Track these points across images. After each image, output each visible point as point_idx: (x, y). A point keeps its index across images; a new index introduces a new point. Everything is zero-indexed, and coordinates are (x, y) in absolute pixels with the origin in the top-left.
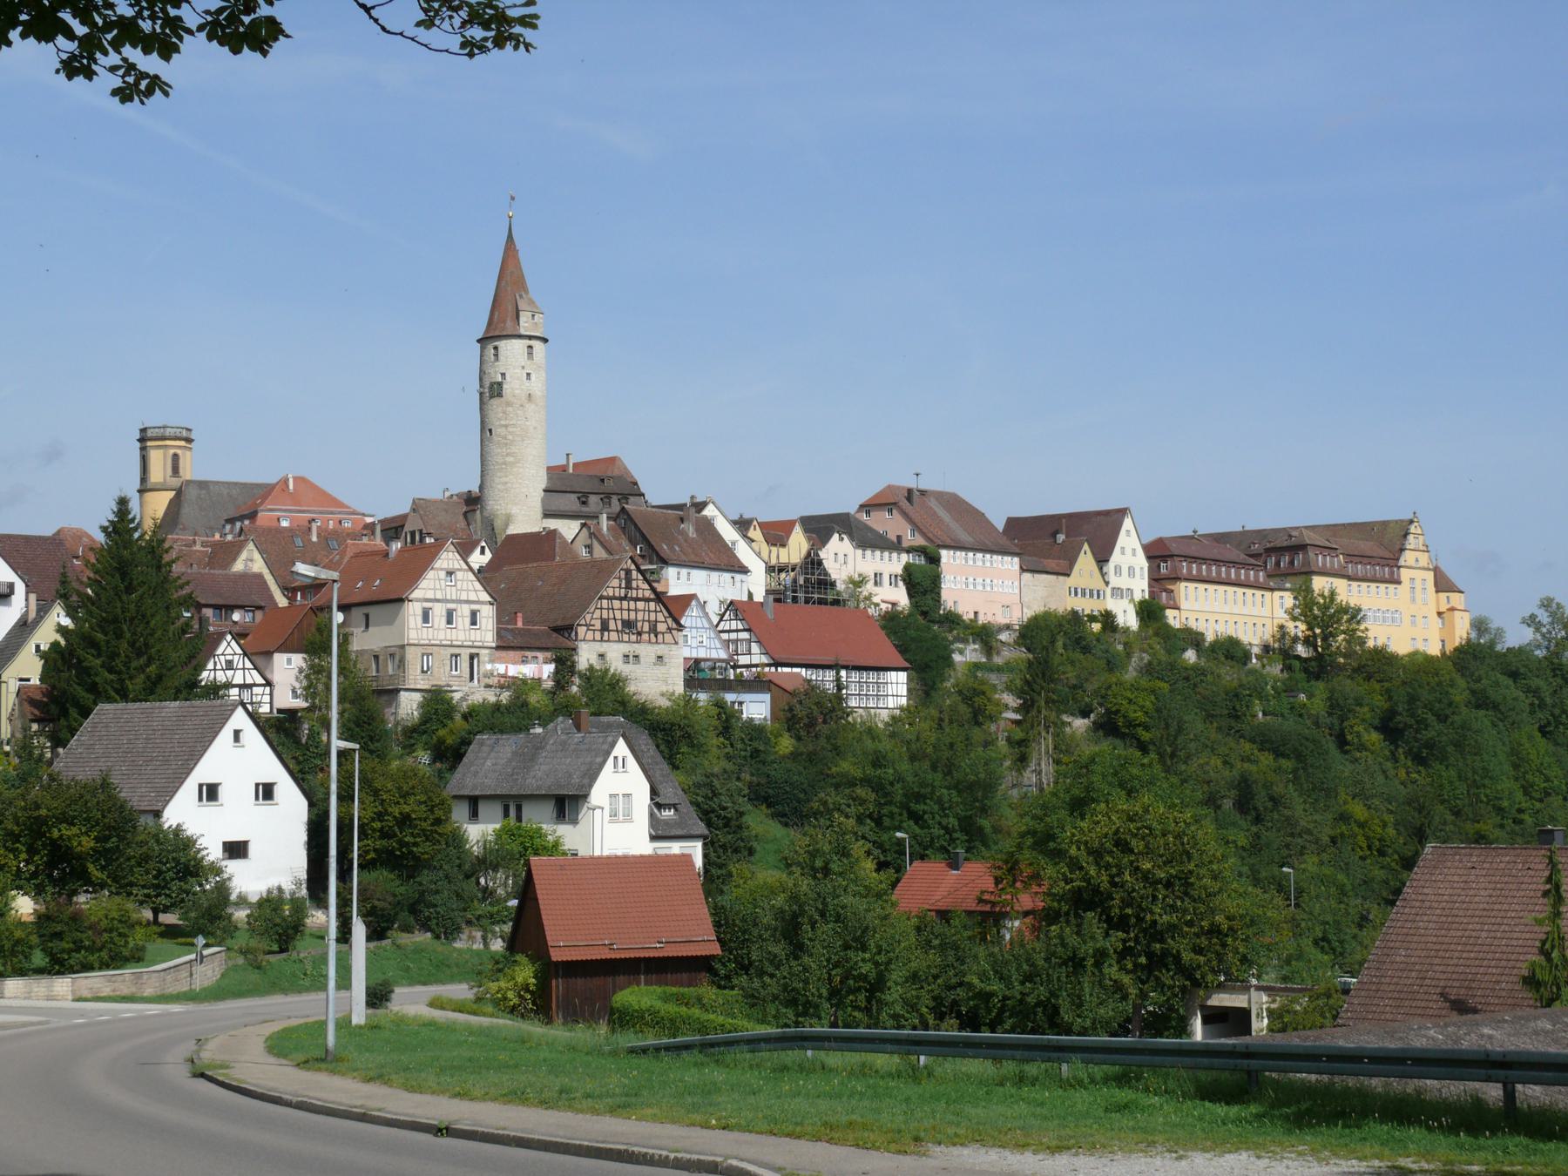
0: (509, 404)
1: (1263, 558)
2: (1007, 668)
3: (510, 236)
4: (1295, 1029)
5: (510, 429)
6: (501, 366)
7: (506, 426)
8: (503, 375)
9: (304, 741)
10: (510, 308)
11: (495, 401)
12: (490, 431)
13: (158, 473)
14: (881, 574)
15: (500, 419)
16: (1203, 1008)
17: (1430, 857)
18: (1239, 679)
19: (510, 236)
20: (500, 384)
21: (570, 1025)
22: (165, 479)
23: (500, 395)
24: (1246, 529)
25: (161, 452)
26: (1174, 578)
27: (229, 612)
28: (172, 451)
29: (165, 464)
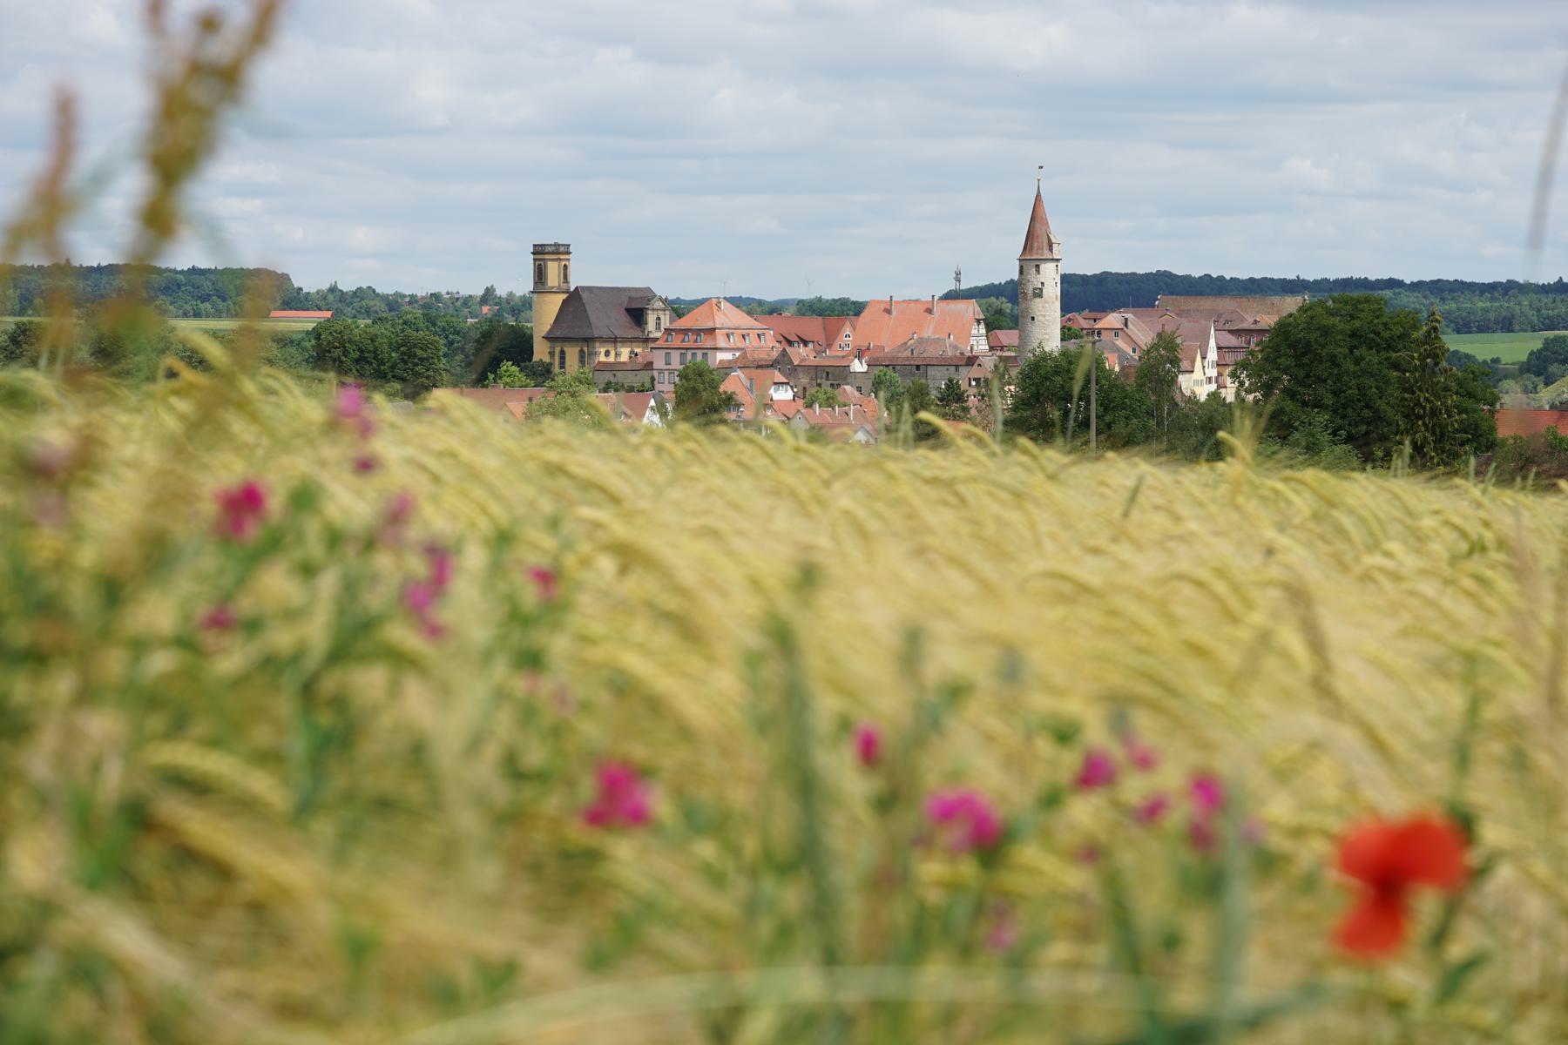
0: (1046, 302)
1: (656, 374)
2: (671, 372)
3: (1038, 197)
4: (616, 390)
7: (1045, 316)
8: (1043, 284)
9: (328, 314)
11: (1038, 300)
12: (1033, 318)
13: (553, 278)
14: (535, 246)
15: (1040, 311)
18: (1329, 434)
19: (1038, 197)
20: (1041, 290)
21: (418, 398)
22: (559, 284)
23: (1040, 296)
25: (556, 263)
26: (1223, 365)
28: (563, 263)
29: (559, 276)
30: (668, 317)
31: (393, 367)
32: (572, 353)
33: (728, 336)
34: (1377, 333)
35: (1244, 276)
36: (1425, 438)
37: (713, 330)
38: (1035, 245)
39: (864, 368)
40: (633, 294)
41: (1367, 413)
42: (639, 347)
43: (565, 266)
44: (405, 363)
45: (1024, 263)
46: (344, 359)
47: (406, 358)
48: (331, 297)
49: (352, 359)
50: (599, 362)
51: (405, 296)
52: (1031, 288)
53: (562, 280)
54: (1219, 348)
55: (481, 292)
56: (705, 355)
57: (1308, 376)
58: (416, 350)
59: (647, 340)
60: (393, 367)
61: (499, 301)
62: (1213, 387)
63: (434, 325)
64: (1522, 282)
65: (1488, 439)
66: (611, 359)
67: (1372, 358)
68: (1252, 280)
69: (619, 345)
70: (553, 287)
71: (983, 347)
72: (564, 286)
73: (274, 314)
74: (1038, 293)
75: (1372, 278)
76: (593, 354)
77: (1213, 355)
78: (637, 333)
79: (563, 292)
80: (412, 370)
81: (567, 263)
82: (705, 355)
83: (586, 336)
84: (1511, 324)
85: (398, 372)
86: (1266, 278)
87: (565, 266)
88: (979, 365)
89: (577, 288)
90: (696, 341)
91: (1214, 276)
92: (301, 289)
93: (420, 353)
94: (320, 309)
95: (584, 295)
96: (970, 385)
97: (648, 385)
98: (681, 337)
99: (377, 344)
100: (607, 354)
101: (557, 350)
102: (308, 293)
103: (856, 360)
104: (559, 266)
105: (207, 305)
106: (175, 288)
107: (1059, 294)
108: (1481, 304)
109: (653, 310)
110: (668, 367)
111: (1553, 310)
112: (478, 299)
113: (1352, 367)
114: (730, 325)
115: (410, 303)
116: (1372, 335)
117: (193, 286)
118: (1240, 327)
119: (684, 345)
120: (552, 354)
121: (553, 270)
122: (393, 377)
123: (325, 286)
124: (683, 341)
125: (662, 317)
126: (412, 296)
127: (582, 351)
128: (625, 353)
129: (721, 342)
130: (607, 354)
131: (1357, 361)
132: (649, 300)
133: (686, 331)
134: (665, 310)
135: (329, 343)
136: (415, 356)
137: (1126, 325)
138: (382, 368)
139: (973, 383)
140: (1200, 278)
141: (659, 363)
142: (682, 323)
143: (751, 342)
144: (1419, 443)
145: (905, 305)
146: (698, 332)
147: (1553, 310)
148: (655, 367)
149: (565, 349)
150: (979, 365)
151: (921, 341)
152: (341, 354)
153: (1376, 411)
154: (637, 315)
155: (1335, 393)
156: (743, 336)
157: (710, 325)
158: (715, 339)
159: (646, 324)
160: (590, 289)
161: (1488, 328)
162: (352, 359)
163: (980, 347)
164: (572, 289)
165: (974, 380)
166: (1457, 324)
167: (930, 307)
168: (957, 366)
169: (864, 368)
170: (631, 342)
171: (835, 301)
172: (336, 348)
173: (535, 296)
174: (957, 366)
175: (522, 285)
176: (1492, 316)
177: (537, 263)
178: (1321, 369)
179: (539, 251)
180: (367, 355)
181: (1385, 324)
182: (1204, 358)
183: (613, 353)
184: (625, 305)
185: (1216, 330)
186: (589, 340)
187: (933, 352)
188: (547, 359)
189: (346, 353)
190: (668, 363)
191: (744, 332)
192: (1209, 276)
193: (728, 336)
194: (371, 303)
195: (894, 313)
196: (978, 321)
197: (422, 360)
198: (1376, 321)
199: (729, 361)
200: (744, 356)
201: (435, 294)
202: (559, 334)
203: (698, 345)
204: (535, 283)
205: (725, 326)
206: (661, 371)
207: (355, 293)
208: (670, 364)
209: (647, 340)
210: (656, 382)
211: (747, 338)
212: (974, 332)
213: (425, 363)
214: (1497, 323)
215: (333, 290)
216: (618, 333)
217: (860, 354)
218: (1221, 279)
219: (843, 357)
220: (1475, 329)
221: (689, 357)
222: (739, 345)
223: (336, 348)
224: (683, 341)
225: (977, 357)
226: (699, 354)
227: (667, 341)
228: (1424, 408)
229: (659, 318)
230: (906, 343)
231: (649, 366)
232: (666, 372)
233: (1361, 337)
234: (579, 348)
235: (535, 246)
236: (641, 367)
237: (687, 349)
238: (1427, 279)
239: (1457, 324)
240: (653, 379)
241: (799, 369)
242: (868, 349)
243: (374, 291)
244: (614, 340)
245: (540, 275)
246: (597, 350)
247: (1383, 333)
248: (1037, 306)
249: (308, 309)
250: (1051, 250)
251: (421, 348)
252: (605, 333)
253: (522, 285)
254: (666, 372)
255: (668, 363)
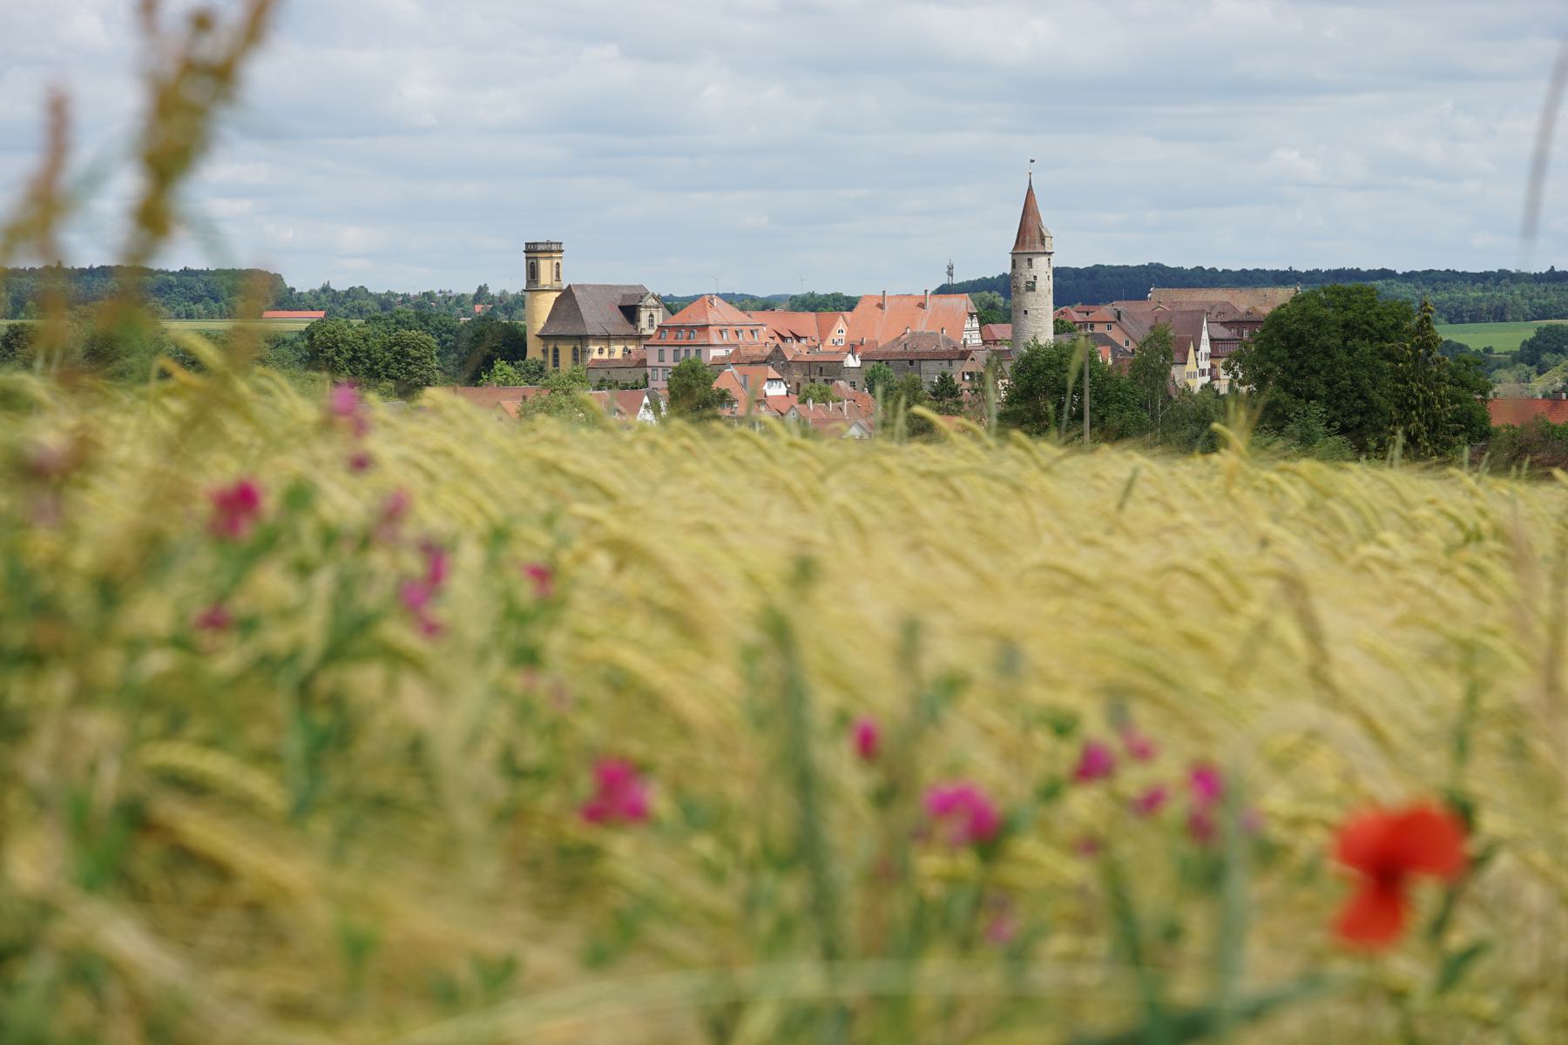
1: (649, 371)
2: (665, 368)
3: (1030, 189)
5: (1040, 311)
6: (1034, 272)
8: (1035, 277)
10: (1037, 234)
11: (1030, 293)
12: (1026, 312)
14: (527, 244)
16: (555, 346)
17: (1443, 392)
19: (1030, 189)
20: (1034, 283)
23: (1033, 289)
24: (1557, 270)
25: (548, 262)
27: (709, 372)
28: (556, 261)
30: (661, 314)
31: (386, 367)
32: (566, 351)
33: (721, 332)
34: (1369, 324)
35: (1236, 268)
36: (1419, 428)
37: (707, 326)
38: (1028, 238)
39: (858, 363)
40: (625, 291)
41: (1360, 404)
42: (630, 345)
43: (558, 264)
44: (399, 362)
45: (1017, 257)
46: (336, 358)
47: (399, 357)
48: (323, 297)
49: (345, 359)
50: (593, 360)
51: (397, 295)
52: (1024, 282)
53: (555, 278)
54: (1212, 340)
55: (474, 291)
56: (698, 352)
57: (1301, 367)
58: (409, 350)
59: (639, 338)
60: (386, 367)
61: (492, 299)
62: (1207, 379)
63: (427, 324)
64: (1513, 271)
65: (1481, 428)
66: (605, 356)
67: (1365, 348)
68: (1244, 271)
69: (612, 342)
70: (545, 286)
71: (977, 341)
72: (557, 285)
73: (267, 314)
74: (1031, 287)
75: (1364, 269)
76: (585, 352)
77: (1205, 347)
78: (630, 330)
79: (556, 291)
80: (405, 369)
81: (559, 261)
82: (698, 352)
83: (579, 333)
84: (1503, 314)
85: (393, 372)
86: (1257, 270)
87: (558, 264)
88: (972, 359)
89: (569, 286)
90: (689, 338)
91: (1206, 268)
92: (293, 289)
93: (413, 352)
94: (313, 310)
95: (577, 293)
96: (963, 379)
97: (641, 382)
98: (674, 334)
99: (370, 343)
100: (601, 351)
101: (551, 348)
102: (301, 294)
103: (850, 356)
104: (552, 264)
105: (200, 306)
106: (167, 289)
107: (1052, 288)
108: (1473, 294)
109: (646, 307)
110: (662, 364)
111: (1545, 298)
112: (471, 298)
113: (1345, 358)
114: (723, 321)
115: (403, 302)
116: (1365, 327)
117: (185, 287)
118: (1233, 318)
119: (679, 342)
120: (545, 352)
121: (545, 268)
122: (387, 376)
123: (318, 286)
124: (676, 338)
125: (655, 314)
126: (404, 295)
127: (575, 349)
128: (618, 351)
129: (715, 339)
130: (601, 351)
131: (1350, 352)
132: (642, 298)
133: (678, 328)
134: (658, 308)
135: (322, 343)
136: (408, 355)
137: (1119, 318)
138: (376, 367)
139: (967, 377)
140: (1192, 270)
141: (652, 360)
142: (675, 320)
143: (745, 338)
144: (1412, 433)
145: (898, 300)
146: (691, 329)
147: (1545, 298)
148: (648, 365)
149: (558, 346)
150: (972, 359)
151: (914, 336)
152: (334, 354)
153: (1369, 401)
154: (630, 312)
155: (1329, 384)
156: (737, 333)
157: (703, 321)
158: (708, 336)
159: (639, 321)
160: (582, 287)
161: (1481, 318)
162: (345, 359)
163: (974, 341)
164: (565, 287)
165: (968, 374)
166: (1449, 313)
167: (922, 301)
168: (950, 360)
169: (858, 363)
170: (624, 339)
171: (828, 296)
172: (329, 348)
173: (528, 294)
174: (950, 360)
175: (515, 283)
176: (1484, 305)
177: (530, 261)
178: (1314, 361)
179: (532, 250)
180: (360, 354)
181: (1378, 315)
182: (1197, 350)
183: (606, 351)
184: (619, 303)
185: (1208, 322)
186: (583, 339)
187: (926, 346)
188: (540, 357)
189: (339, 353)
190: (661, 360)
191: (738, 328)
192: (1201, 268)
193: (721, 332)
194: (363, 303)
195: (887, 308)
196: (971, 315)
197: (416, 359)
198: (1368, 312)
199: (722, 358)
200: (737, 352)
201: (428, 293)
202: (552, 332)
203: (692, 341)
204: (528, 282)
205: (718, 322)
206: (654, 368)
207: (348, 293)
208: (663, 361)
209: (639, 338)
210: (649, 379)
211: (725, 334)
212: (967, 326)
213: (418, 362)
214: (1489, 312)
215: (325, 289)
216: (611, 330)
217: (853, 350)
218: (1213, 270)
219: (837, 352)
220: (1468, 319)
221: (682, 354)
222: (733, 341)
223: (329, 348)
224: (676, 338)
225: (971, 351)
226: (693, 351)
227: (660, 338)
228: (1417, 398)
229: (651, 315)
230: (899, 338)
231: (642, 363)
232: (660, 370)
233: (1354, 327)
234: (572, 347)
235: (527, 244)
236: (634, 364)
237: (680, 346)
238: (1419, 269)
239: (1449, 313)
240: (646, 376)
241: (793, 365)
242: (862, 344)
243: (366, 291)
244: (608, 338)
245: (533, 272)
246: (591, 347)
247: (1375, 324)
248: (1030, 300)
249: (300, 310)
250: (1043, 245)
251: (414, 348)
252: (598, 331)
253: (515, 283)
254: (660, 370)
255: (661, 360)
